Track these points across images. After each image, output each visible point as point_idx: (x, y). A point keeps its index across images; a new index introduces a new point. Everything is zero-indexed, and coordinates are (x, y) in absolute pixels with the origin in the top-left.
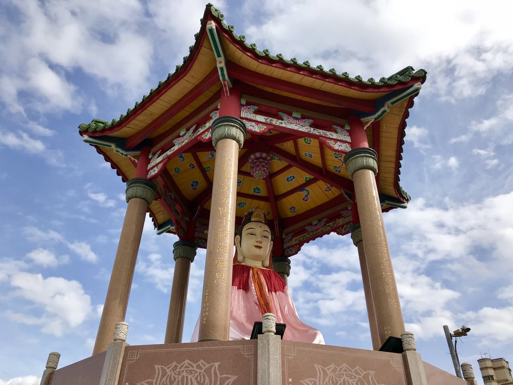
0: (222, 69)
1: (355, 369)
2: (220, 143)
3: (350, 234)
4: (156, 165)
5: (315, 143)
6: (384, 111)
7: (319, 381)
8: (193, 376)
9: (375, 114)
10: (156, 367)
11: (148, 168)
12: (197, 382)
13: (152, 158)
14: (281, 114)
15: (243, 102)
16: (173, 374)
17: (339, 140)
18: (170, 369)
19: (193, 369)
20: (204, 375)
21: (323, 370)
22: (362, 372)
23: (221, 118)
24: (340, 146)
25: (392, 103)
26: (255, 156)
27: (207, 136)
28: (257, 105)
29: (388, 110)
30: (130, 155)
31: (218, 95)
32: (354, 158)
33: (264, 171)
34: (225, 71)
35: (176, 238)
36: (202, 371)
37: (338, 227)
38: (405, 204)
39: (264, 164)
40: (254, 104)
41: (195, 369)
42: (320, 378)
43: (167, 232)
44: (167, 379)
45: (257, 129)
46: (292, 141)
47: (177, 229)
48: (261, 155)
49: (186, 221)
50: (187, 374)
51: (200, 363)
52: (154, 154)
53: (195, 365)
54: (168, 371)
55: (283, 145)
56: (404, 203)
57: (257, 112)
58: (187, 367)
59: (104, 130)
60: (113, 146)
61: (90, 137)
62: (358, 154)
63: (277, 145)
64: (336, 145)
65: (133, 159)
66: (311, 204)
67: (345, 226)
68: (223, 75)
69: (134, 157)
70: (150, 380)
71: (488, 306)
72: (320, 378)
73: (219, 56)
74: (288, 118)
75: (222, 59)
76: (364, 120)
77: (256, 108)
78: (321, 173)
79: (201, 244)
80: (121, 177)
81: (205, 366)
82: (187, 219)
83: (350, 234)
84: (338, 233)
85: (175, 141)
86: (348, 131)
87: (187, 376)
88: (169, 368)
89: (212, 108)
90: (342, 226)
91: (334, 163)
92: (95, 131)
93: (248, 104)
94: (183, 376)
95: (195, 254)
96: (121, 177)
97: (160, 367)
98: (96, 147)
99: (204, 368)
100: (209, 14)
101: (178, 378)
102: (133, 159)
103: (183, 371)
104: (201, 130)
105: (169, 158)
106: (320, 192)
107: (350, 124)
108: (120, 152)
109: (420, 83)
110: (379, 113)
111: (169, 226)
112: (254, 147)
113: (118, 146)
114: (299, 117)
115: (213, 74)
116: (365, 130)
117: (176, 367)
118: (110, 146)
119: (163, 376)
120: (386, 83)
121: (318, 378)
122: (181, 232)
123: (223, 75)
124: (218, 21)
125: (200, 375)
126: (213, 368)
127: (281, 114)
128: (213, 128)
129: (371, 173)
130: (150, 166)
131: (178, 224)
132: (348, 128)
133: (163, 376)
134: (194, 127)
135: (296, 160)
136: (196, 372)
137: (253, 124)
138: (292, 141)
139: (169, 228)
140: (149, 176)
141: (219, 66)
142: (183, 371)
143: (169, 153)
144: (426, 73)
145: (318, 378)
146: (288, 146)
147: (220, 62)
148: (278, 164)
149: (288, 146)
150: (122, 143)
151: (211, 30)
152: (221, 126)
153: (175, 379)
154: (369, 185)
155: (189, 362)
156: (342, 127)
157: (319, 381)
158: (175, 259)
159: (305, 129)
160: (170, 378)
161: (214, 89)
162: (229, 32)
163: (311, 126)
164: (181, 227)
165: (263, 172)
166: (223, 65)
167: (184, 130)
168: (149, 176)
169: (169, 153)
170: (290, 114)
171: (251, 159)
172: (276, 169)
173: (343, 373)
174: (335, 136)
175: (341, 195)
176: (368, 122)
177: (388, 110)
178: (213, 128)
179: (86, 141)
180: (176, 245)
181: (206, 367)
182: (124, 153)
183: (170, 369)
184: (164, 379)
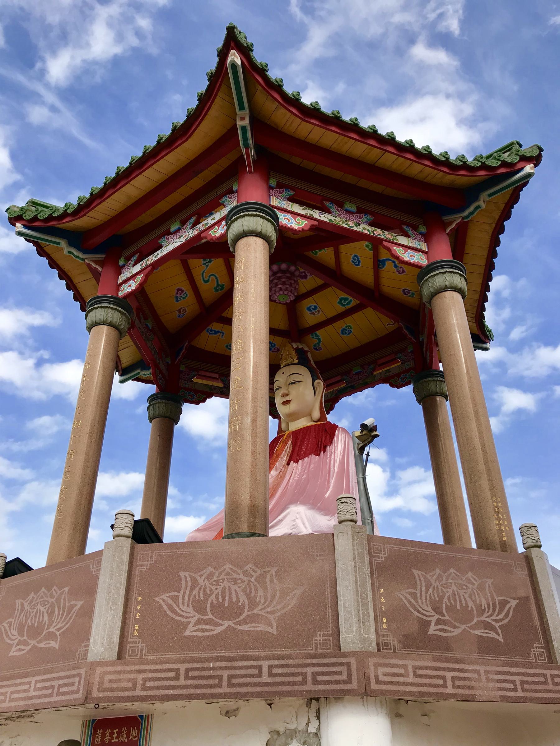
0: (244, 128)
1: (466, 576)
2: (242, 243)
3: (411, 386)
4: (133, 277)
5: (363, 250)
6: (478, 207)
7: (184, 596)
8: (239, 587)
9: (463, 210)
10: (182, 574)
11: (120, 281)
12: (246, 594)
13: (124, 265)
14: (328, 204)
15: (273, 183)
16: (208, 586)
17: (410, 250)
18: (203, 577)
19: (238, 576)
20: (255, 586)
21: (425, 578)
22: (476, 581)
23: (241, 205)
24: (411, 256)
25: (490, 195)
26: (279, 268)
27: (218, 232)
28: (292, 189)
29: (483, 206)
30: (89, 258)
31: (235, 171)
32: (432, 276)
33: (281, 289)
34: (251, 130)
35: (152, 389)
36: (253, 580)
37: (392, 377)
38: (488, 345)
39: (293, 282)
40: (287, 187)
41: (241, 576)
42: (184, 593)
43: (133, 380)
44: (199, 592)
45: (296, 224)
46: (332, 248)
47: (154, 374)
48: (279, 268)
49: (168, 363)
50: (229, 584)
51: (247, 567)
52: (128, 259)
53: (240, 572)
54: (200, 580)
55: (316, 254)
56: (486, 343)
57: (291, 199)
58: (228, 574)
59: (50, 218)
60: (63, 244)
61: (25, 226)
62: (434, 271)
63: (310, 254)
64: (406, 255)
65: (93, 265)
66: (352, 341)
67: (402, 376)
68: (245, 139)
69: (96, 262)
70: (176, 594)
71: (303, 503)
72: (184, 593)
73: (242, 108)
74: (338, 211)
75: (247, 112)
76: (446, 218)
77: (291, 193)
78: (370, 296)
79: (189, 398)
80: (72, 293)
81: (256, 572)
82: (168, 360)
83: (411, 386)
84: (392, 385)
85: (161, 240)
86: (423, 235)
87: (230, 588)
88: (201, 576)
89: (224, 190)
90: (398, 375)
91: (392, 283)
92: (35, 219)
93: (280, 186)
94: (224, 588)
95: (181, 412)
96: (72, 293)
97: (187, 574)
98: (36, 244)
99: (255, 575)
100: (232, 39)
101: (216, 589)
102: (93, 265)
103: (223, 580)
104: (210, 221)
105: (155, 265)
106: (369, 324)
107: (425, 224)
108: (73, 254)
109: (532, 165)
110: (471, 209)
111: (139, 371)
112: (287, 252)
113: (71, 244)
114: (353, 208)
115: (229, 136)
116: (448, 234)
117: (211, 575)
118: (59, 244)
119: (193, 588)
120: (483, 163)
121: (419, 587)
122: (161, 379)
123: (245, 139)
124: (246, 51)
125: (250, 586)
126: (268, 576)
127: (328, 204)
128: (229, 219)
129: (457, 296)
130: (121, 278)
131: (156, 366)
132: (423, 229)
133: (193, 588)
134: (194, 219)
135: (335, 277)
136: (243, 581)
137: (289, 216)
138: (332, 248)
139: (139, 373)
140: (121, 294)
141: (239, 123)
142: (223, 580)
143: (152, 259)
144: (541, 150)
145: (419, 587)
146: (326, 255)
147: (243, 119)
148: (310, 281)
149: (326, 255)
150: (80, 240)
151: (234, 65)
152: (237, 218)
153: (211, 590)
154: (453, 315)
155: (231, 566)
156: (415, 228)
157: (184, 596)
158: (151, 419)
159: (364, 228)
160: (205, 590)
161: (230, 158)
162: (262, 71)
163: (371, 224)
164: (161, 372)
165: (281, 292)
166: (246, 122)
167: (178, 222)
168: (121, 294)
169: (152, 259)
170: (340, 205)
171: (289, 267)
172: (303, 290)
173: (451, 581)
174: (403, 240)
175: (399, 329)
176: (451, 223)
177: (483, 206)
178: (229, 219)
179: (20, 234)
180: (152, 399)
181: (257, 574)
182: (81, 255)
183: (203, 577)
184: (195, 592)
